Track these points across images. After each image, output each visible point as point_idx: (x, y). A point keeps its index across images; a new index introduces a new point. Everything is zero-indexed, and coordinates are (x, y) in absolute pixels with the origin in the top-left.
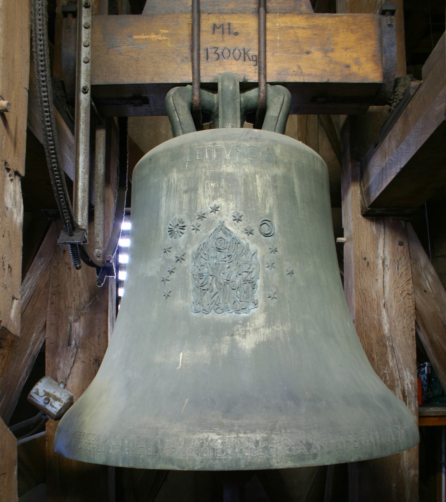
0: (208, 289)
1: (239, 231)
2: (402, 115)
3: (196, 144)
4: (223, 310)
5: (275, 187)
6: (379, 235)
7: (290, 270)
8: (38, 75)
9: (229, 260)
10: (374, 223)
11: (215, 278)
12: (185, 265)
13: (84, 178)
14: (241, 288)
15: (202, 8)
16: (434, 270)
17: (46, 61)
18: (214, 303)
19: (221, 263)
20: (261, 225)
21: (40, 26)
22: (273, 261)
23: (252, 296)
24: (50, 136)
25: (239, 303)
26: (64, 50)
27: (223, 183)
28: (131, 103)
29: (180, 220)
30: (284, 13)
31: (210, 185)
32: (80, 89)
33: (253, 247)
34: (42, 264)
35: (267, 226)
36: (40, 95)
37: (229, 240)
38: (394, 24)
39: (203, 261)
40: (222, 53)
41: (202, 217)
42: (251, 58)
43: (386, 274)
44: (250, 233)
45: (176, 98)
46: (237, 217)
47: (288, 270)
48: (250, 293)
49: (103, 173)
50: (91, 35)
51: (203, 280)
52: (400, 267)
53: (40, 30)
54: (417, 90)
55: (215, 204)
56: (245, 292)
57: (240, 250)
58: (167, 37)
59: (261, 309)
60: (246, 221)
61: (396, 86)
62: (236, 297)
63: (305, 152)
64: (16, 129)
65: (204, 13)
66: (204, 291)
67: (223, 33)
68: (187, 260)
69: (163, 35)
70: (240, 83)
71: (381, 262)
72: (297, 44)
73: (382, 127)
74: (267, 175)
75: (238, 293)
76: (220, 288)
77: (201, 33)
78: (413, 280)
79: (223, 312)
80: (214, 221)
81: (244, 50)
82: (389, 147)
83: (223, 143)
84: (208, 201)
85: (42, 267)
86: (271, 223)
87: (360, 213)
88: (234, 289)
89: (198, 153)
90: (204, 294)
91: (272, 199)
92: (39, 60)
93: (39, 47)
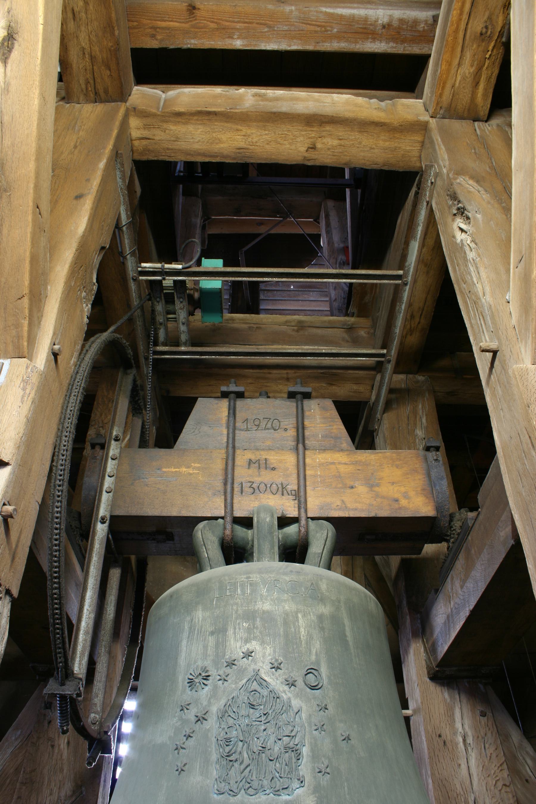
0: (236, 760)
1: (278, 682)
2: (462, 550)
3: (227, 578)
4: (257, 791)
5: (322, 629)
6: (454, 703)
7: (346, 734)
8: (54, 489)
9: (265, 720)
10: (446, 688)
11: (246, 744)
12: (208, 727)
13: (89, 618)
14: (281, 758)
15: (237, 445)
16: (532, 749)
17: (66, 476)
18: (244, 780)
19: (254, 723)
20: (306, 675)
21: (65, 442)
22: (323, 721)
23: (297, 769)
24: (55, 556)
25: (279, 781)
26: (86, 479)
27: (258, 622)
28: (154, 539)
29: (204, 668)
30: (324, 450)
31: (243, 625)
32: (97, 518)
33: (296, 703)
34: (16, 739)
35: (314, 677)
36: (53, 510)
37: (265, 693)
38: (440, 459)
39: (231, 721)
40: (258, 487)
41: (231, 664)
42: (290, 492)
43: (470, 757)
44: (292, 685)
45: (206, 532)
46: (276, 665)
47: (343, 734)
48: (294, 764)
49: (112, 618)
50: (118, 467)
51: (231, 747)
52: (487, 746)
53: (65, 446)
54: (475, 520)
55: (248, 648)
56: (286, 765)
57: (279, 706)
58: (199, 470)
59: (309, 790)
60: (287, 669)
61: (451, 520)
62: (274, 772)
63: (355, 589)
64: (18, 541)
65: (239, 449)
66: (231, 763)
67: (259, 468)
68: (209, 720)
69: (194, 468)
70: (278, 518)
71: (461, 740)
72: (339, 479)
73: (442, 568)
74: (311, 614)
75: (278, 765)
76: (253, 759)
77: (236, 468)
78: (507, 764)
79: (257, 794)
80: (246, 669)
81: (282, 484)
82: (452, 589)
83: (258, 576)
84: (239, 644)
85: (17, 743)
86: (319, 673)
87: (427, 676)
88: (271, 760)
89: (228, 588)
90: (231, 767)
91: (318, 642)
92: (57, 474)
93: (61, 462)
